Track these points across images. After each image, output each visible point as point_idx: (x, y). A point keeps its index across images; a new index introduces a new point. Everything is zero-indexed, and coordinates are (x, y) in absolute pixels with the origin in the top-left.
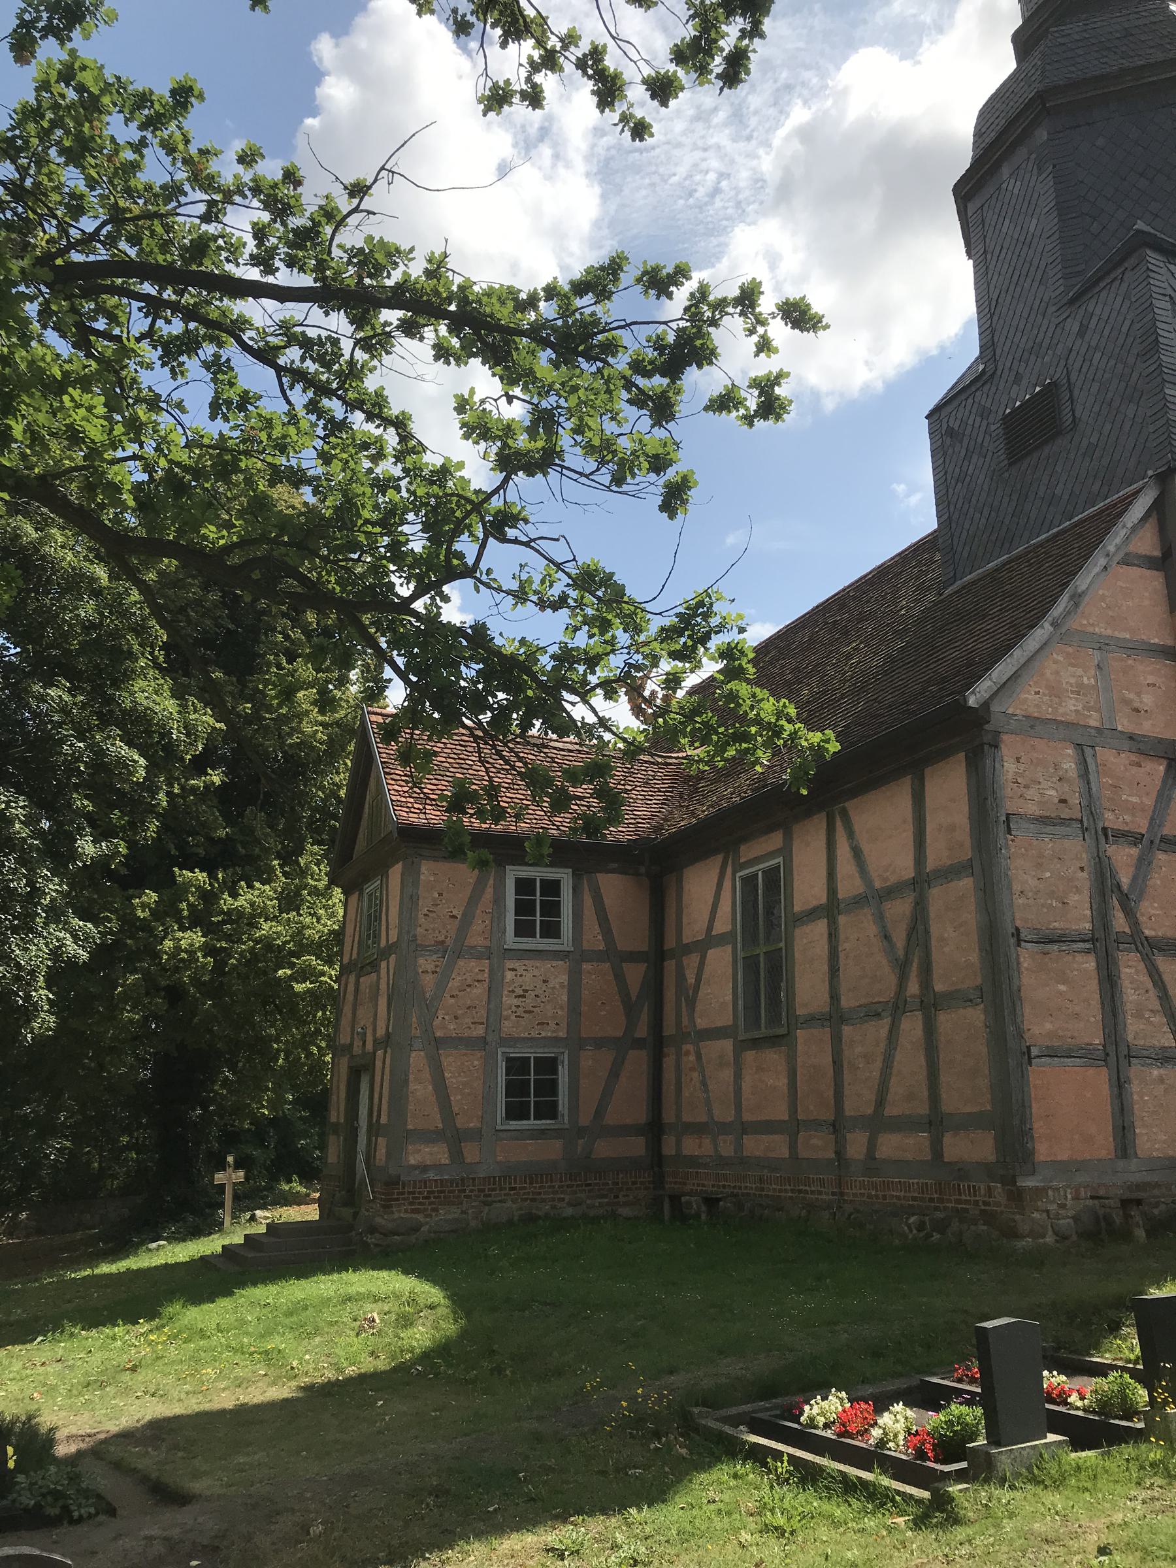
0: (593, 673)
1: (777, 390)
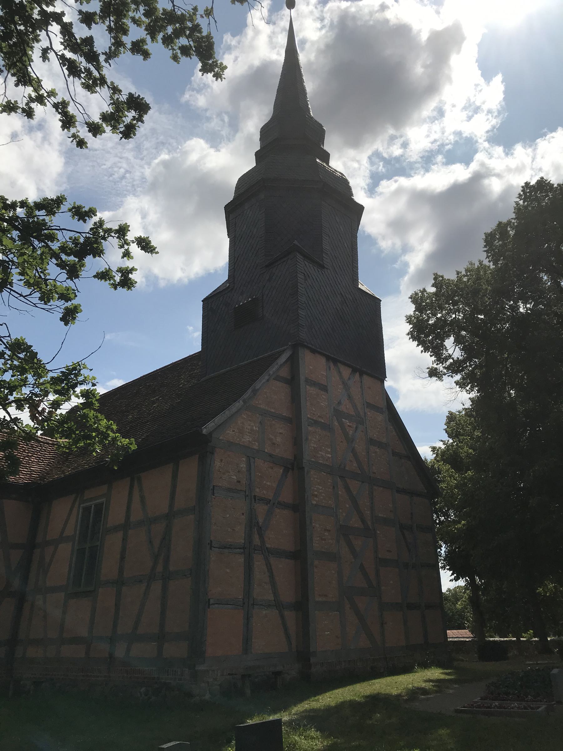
0: (12, 395)
1: (130, 276)
